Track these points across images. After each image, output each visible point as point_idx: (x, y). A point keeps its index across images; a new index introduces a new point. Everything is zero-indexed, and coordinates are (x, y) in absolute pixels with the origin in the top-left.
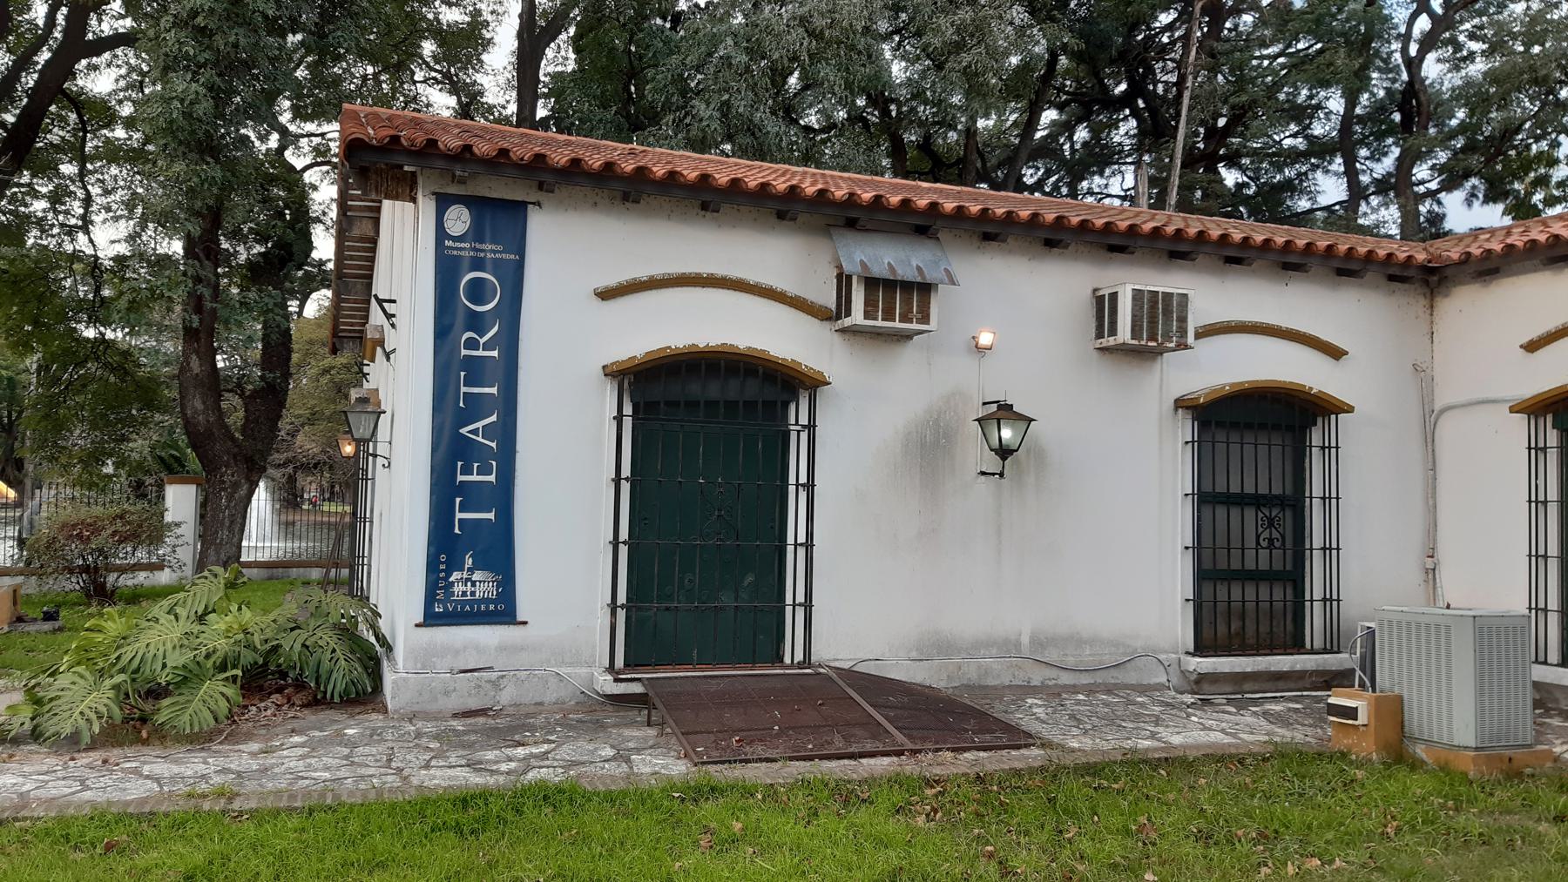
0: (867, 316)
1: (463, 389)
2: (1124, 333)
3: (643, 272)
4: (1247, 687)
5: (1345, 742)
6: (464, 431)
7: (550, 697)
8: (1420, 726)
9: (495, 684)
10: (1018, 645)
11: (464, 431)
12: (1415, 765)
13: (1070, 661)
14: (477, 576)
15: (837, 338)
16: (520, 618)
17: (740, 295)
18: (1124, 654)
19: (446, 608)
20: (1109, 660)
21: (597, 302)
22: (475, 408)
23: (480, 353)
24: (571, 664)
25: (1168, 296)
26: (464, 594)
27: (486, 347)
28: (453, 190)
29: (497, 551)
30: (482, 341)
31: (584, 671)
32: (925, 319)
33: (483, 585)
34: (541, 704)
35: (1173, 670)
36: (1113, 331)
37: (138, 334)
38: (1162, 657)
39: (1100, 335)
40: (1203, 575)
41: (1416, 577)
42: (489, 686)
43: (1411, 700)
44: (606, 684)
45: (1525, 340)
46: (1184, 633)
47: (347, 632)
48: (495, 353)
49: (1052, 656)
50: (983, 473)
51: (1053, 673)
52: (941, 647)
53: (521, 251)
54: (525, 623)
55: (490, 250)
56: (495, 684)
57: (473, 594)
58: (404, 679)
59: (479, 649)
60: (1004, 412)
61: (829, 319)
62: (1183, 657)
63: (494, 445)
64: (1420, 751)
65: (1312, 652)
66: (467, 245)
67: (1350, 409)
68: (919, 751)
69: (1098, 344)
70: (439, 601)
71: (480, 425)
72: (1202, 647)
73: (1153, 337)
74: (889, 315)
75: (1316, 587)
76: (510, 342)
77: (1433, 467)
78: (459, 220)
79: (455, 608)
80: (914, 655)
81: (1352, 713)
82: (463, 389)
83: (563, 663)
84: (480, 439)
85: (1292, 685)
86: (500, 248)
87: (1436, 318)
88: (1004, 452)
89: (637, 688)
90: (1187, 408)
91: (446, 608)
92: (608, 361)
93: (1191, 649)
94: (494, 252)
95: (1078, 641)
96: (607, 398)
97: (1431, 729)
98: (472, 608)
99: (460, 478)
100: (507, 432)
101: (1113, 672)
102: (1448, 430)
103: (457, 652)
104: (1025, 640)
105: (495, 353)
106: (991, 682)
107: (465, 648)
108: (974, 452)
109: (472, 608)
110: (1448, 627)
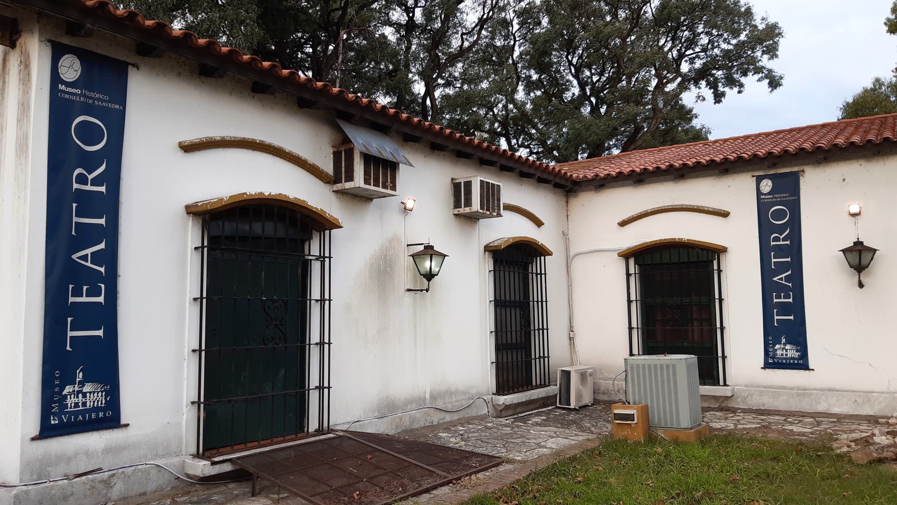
0: (367, 181)
1: (75, 219)
2: (476, 205)
3: (217, 133)
4: (518, 410)
5: (622, 434)
6: (74, 257)
7: (151, 487)
8: (659, 420)
9: (107, 483)
10: (424, 399)
11: (74, 257)
12: (661, 442)
13: (449, 407)
14: (87, 388)
15: (333, 195)
16: (123, 422)
17: (265, 158)
18: (469, 399)
19: (61, 420)
20: (465, 403)
21: (180, 153)
22: (88, 236)
23: (89, 188)
24: (163, 456)
25: (493, 185)
26: (77, 405)
27: (95, 182)
28: (65, 40)
29: (103, 363)
30: (90, 177)
31: (176, 460)
32: (394, 188)
33: (93, 395)
34: (144, 494)
35: (490, 405)
36: (468, 203)
37: (568, 81)
38: (485, 398)
39: (457, 205)
40: (499, 348)
41: (566, 341)
42: (101, 486)
43: (652, 407)
44: (203, 468)
45: (620, 220)
46: (490, 382)
47: (756, 456)
48: (103, 189)
49: (440, 404)
50: (409, 290)
51: (441, 415)
52: (388, 408)
53: (123, 102)
54: (127, 425)
55: (98, 98)
56: (107, 483)
57: (84, 404)
58: (26, 492)
59: (88, 454)
60: (429, 251)
61: (329, 183)
62: (494, 397)
63: (102, 270)
64: (661, 434)
65: (537, 387)
66: (78, 91)
67: (550, 254)
68: (460, 478)
69: (456, 211)
70: (55, 414)
71: (89, 251)
72: (501, 389)
73: (488, 210)
74: (376, 184)
75: (535, 352)
76: (113, 179)
77: (570, 286)
78: (71, 68)
79: (70, 418)
80: (376, 414)
81: (630, 417)
82: (75, 219)
83: (157, 456)
84: (89, 264)
85: (524, 409)
86: (106, 98)
87: (570, 209)
88: (430, 276)
89: (227, 468)
90: (490, 251)
91: (61, 420)
92: (190, 201)
93: (495, 391)
94: (102, 101)
95: (450, 393)
96: (192, 235)
97: (666, 420)
98: (84, 417)
99: (72, 299)
100: (110, 258)
101: (467, 410)
102: (578, 266)
103: (69, 460)
104: (428, 396)
105: (103, 189)
106: (416, 426)
107: (76, 454)
108: (404, 274)
109: (84, 417)
110: (674, 366)
